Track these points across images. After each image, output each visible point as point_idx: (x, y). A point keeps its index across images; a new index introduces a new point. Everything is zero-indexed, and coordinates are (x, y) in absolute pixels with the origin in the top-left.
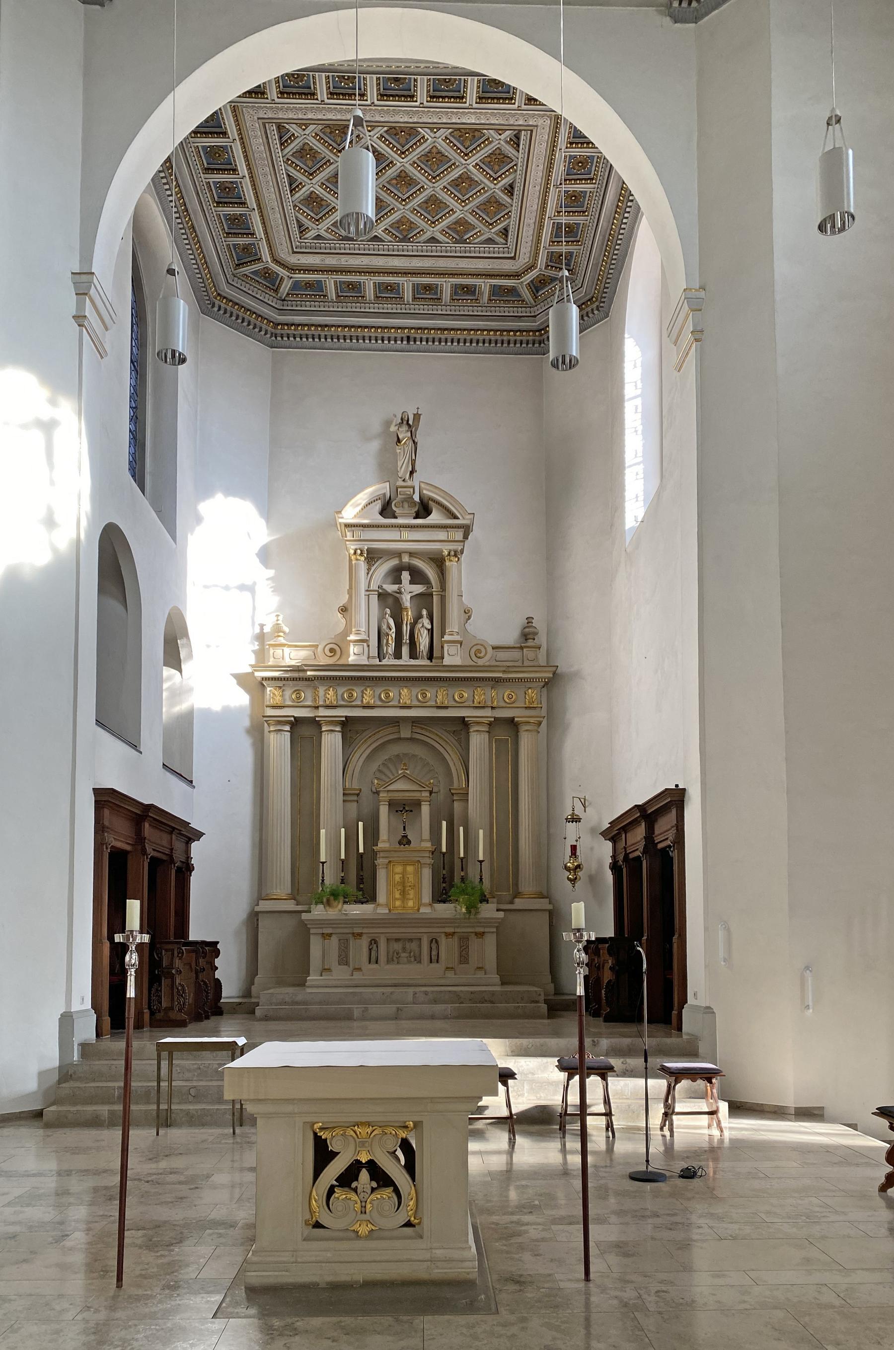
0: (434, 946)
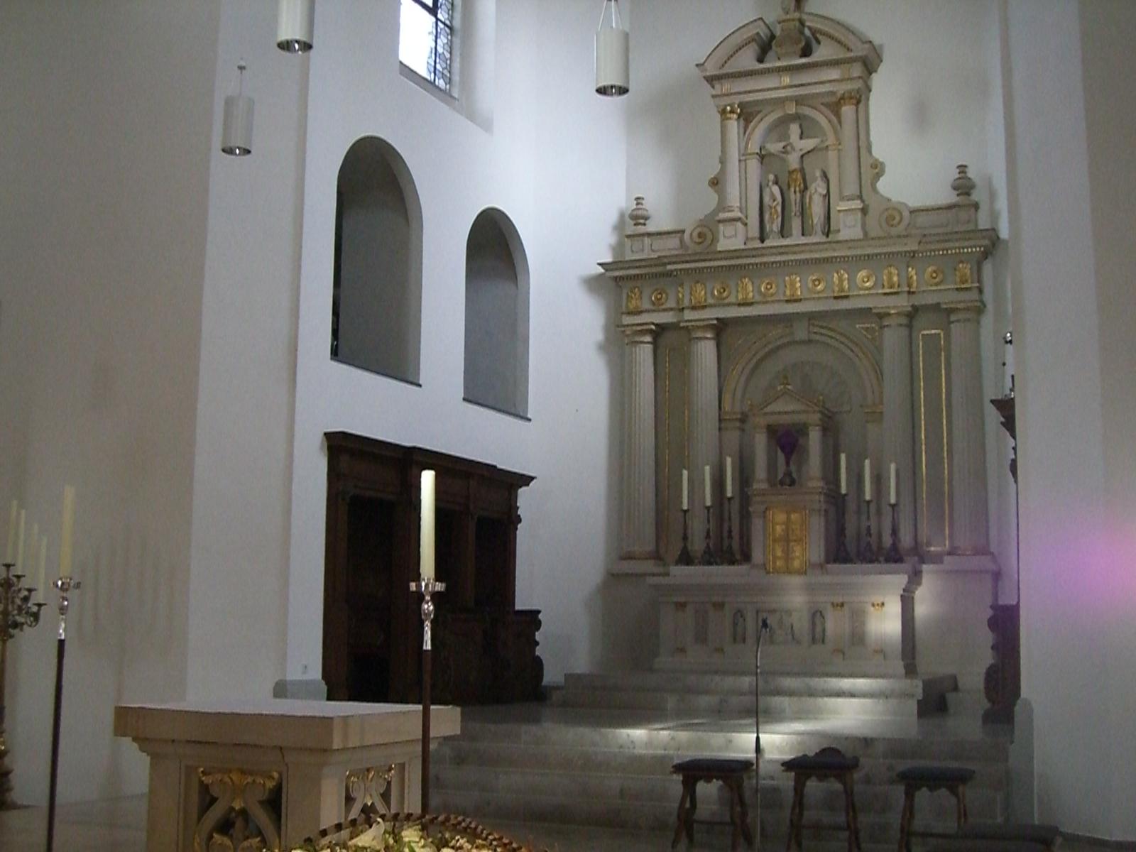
0: (818, 621)
